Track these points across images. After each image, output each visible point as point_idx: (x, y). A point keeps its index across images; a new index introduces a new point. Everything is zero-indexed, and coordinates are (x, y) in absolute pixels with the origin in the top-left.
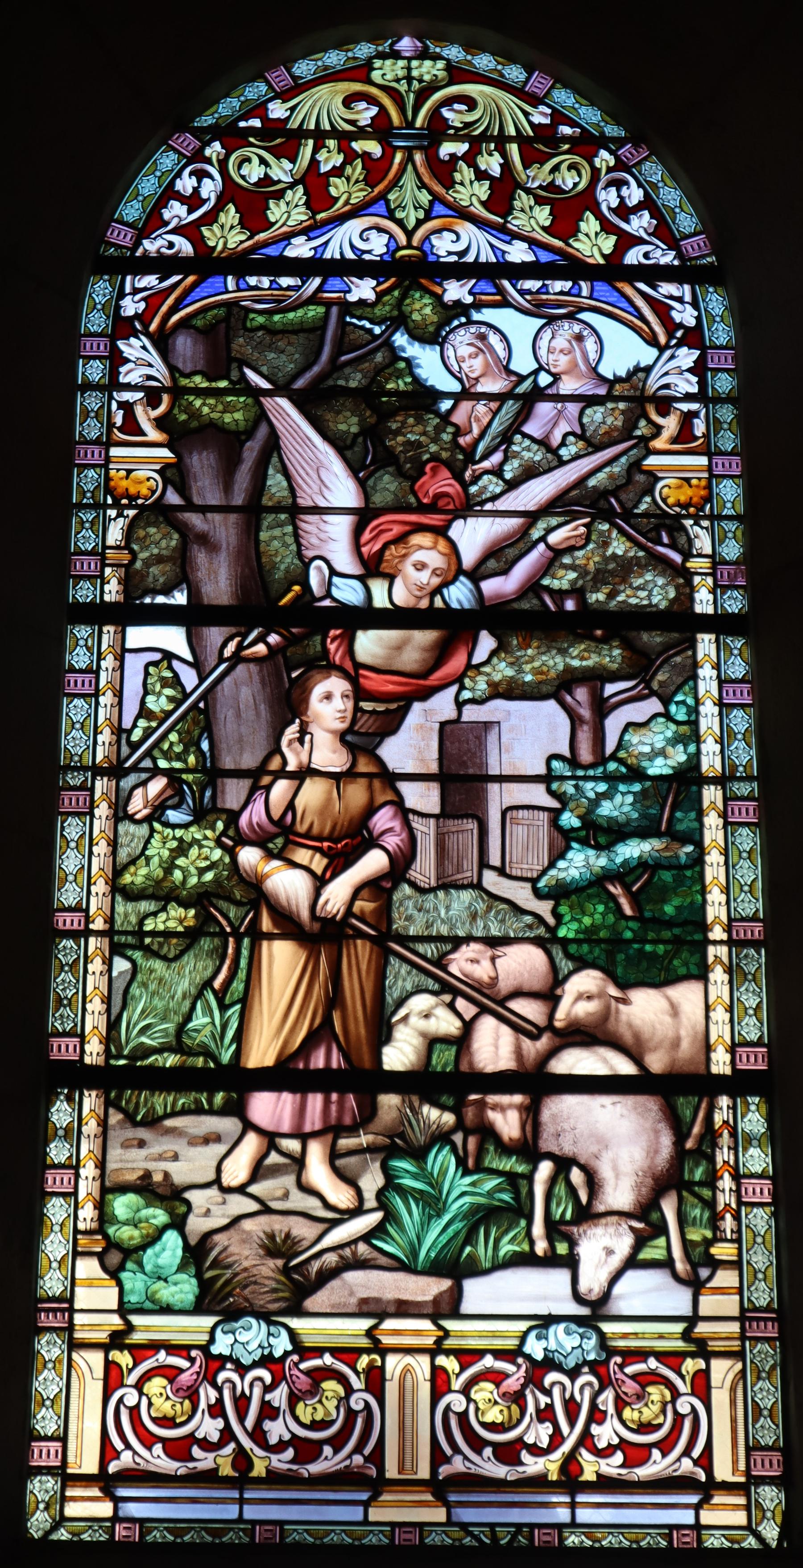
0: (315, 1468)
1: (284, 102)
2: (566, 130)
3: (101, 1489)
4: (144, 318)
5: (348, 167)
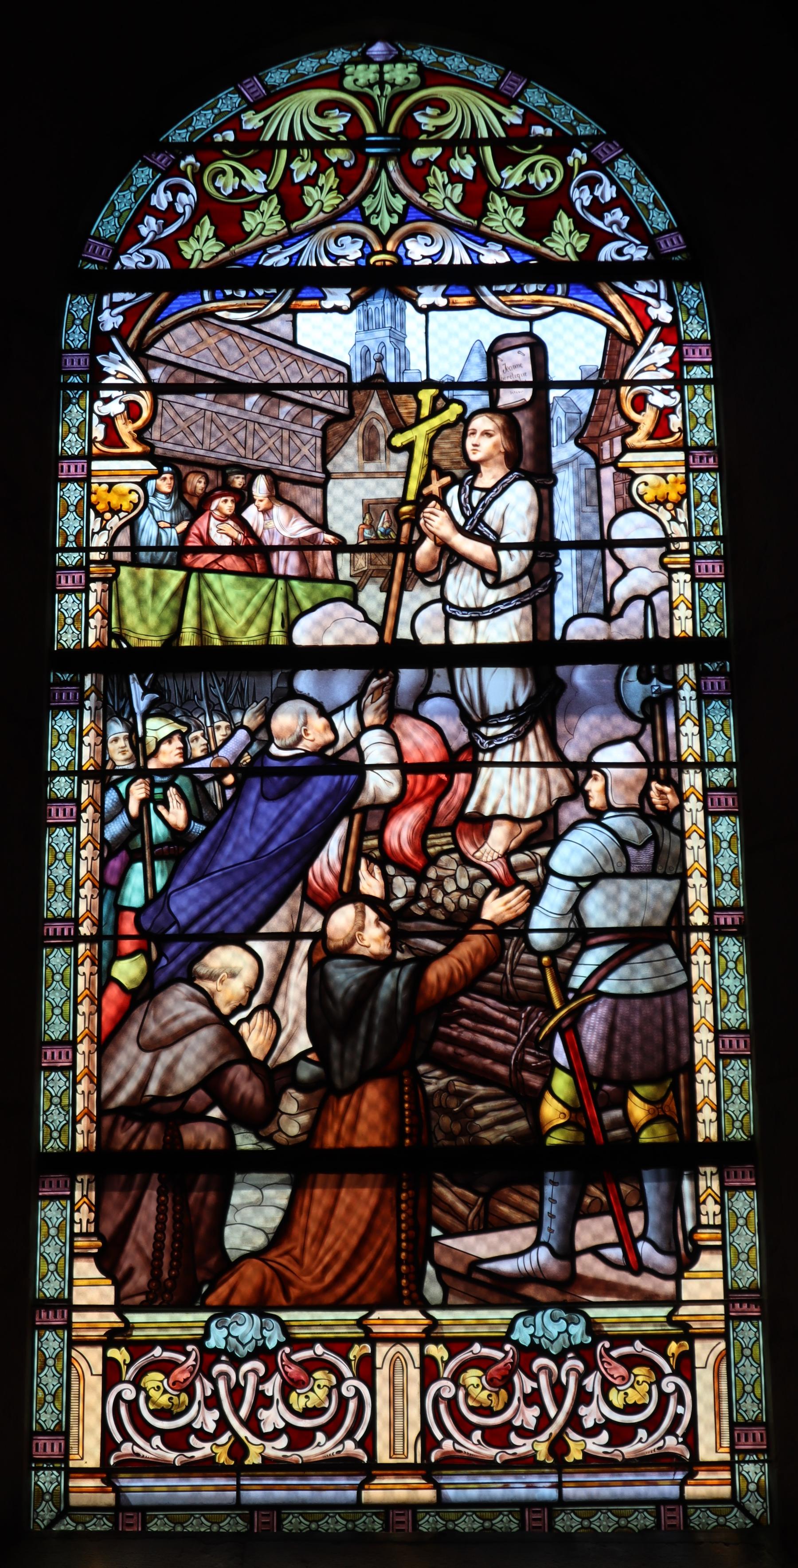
0: (628, 1450)
1: (258, 112)
2: (538, 130)
4: (121, 333)
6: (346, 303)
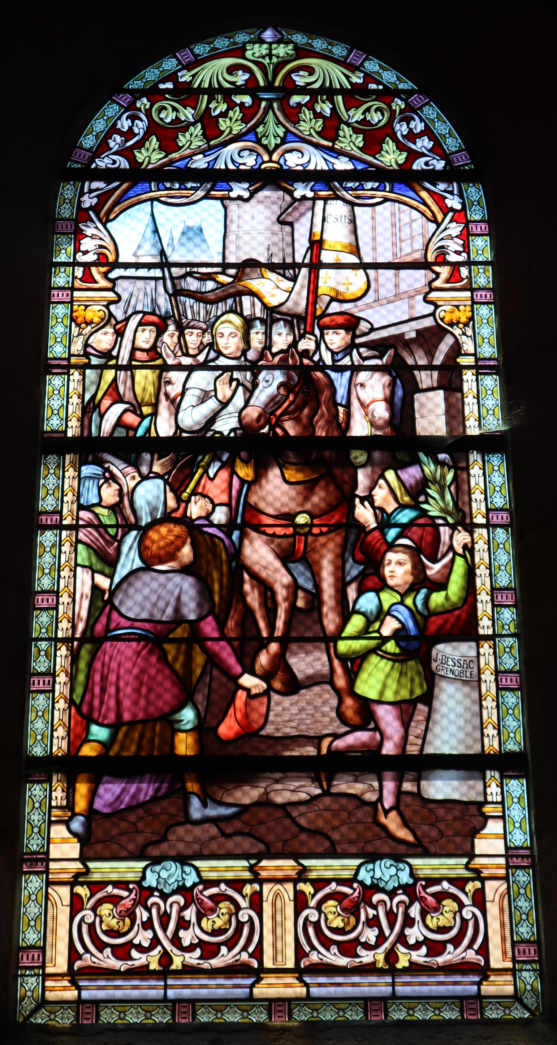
0: (440, 960)
2: (373, 86)
3: (69, 981)
4: (96, 209)
5: (230, 112)
6: (246, 195)
